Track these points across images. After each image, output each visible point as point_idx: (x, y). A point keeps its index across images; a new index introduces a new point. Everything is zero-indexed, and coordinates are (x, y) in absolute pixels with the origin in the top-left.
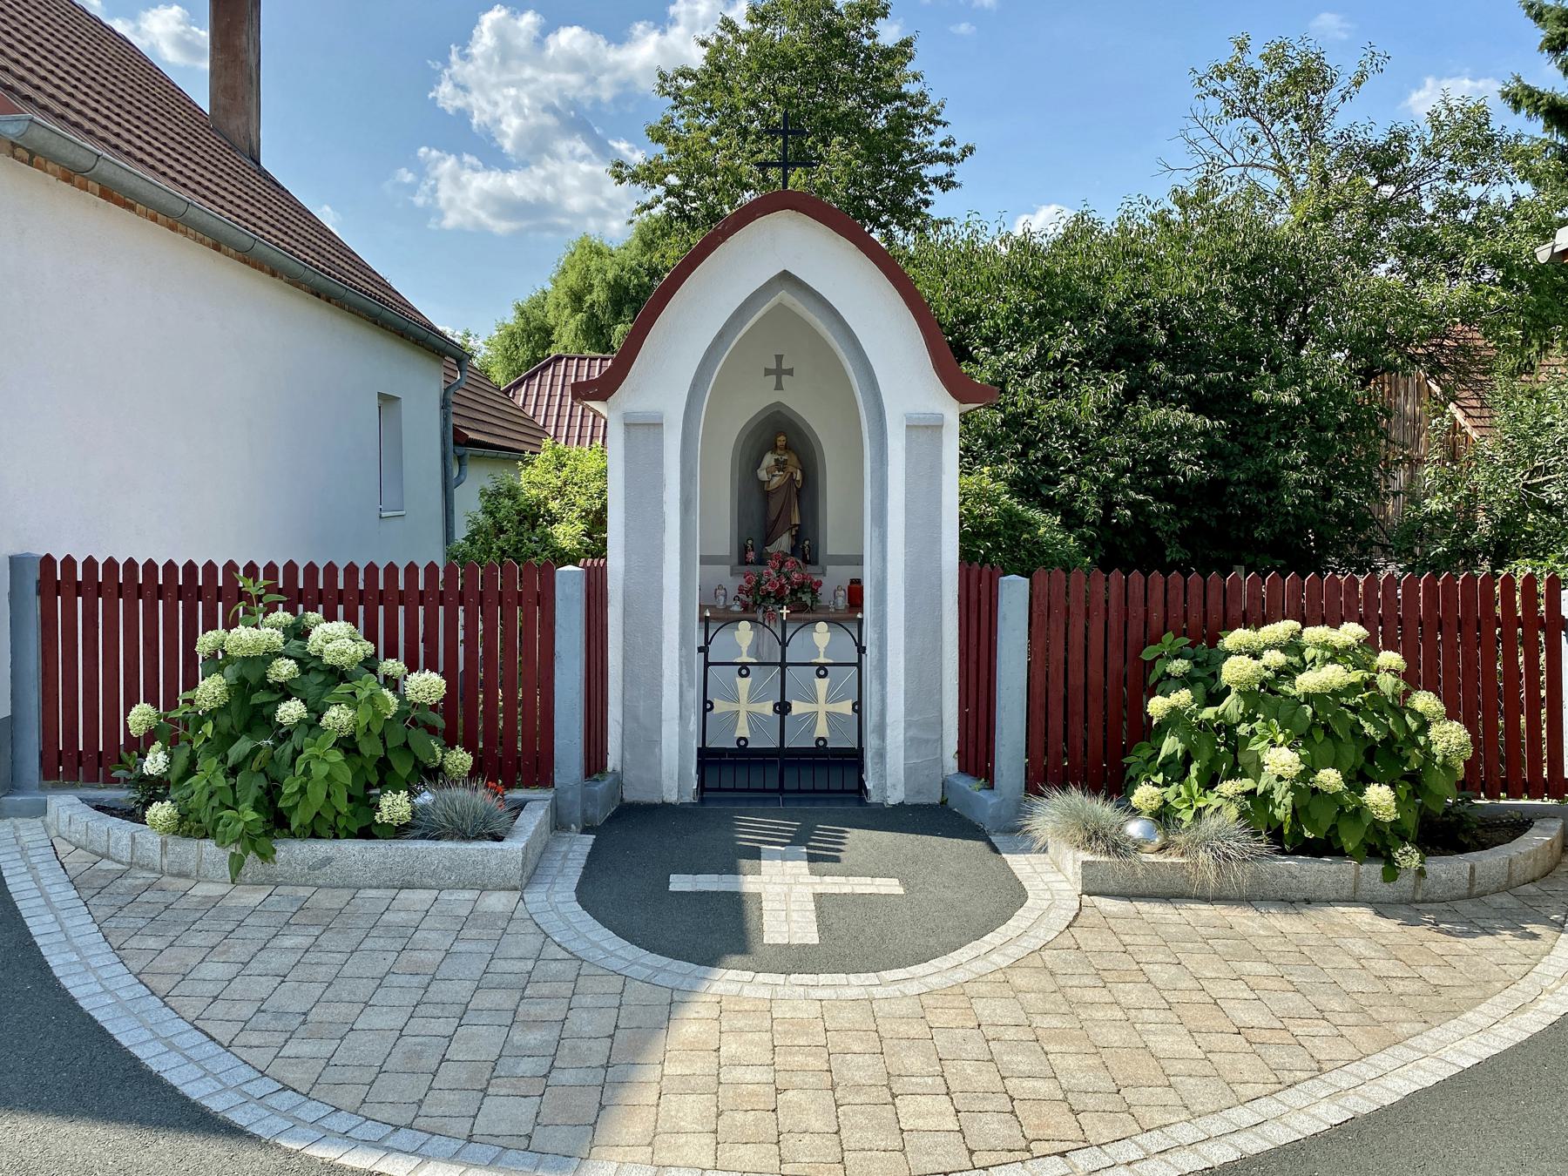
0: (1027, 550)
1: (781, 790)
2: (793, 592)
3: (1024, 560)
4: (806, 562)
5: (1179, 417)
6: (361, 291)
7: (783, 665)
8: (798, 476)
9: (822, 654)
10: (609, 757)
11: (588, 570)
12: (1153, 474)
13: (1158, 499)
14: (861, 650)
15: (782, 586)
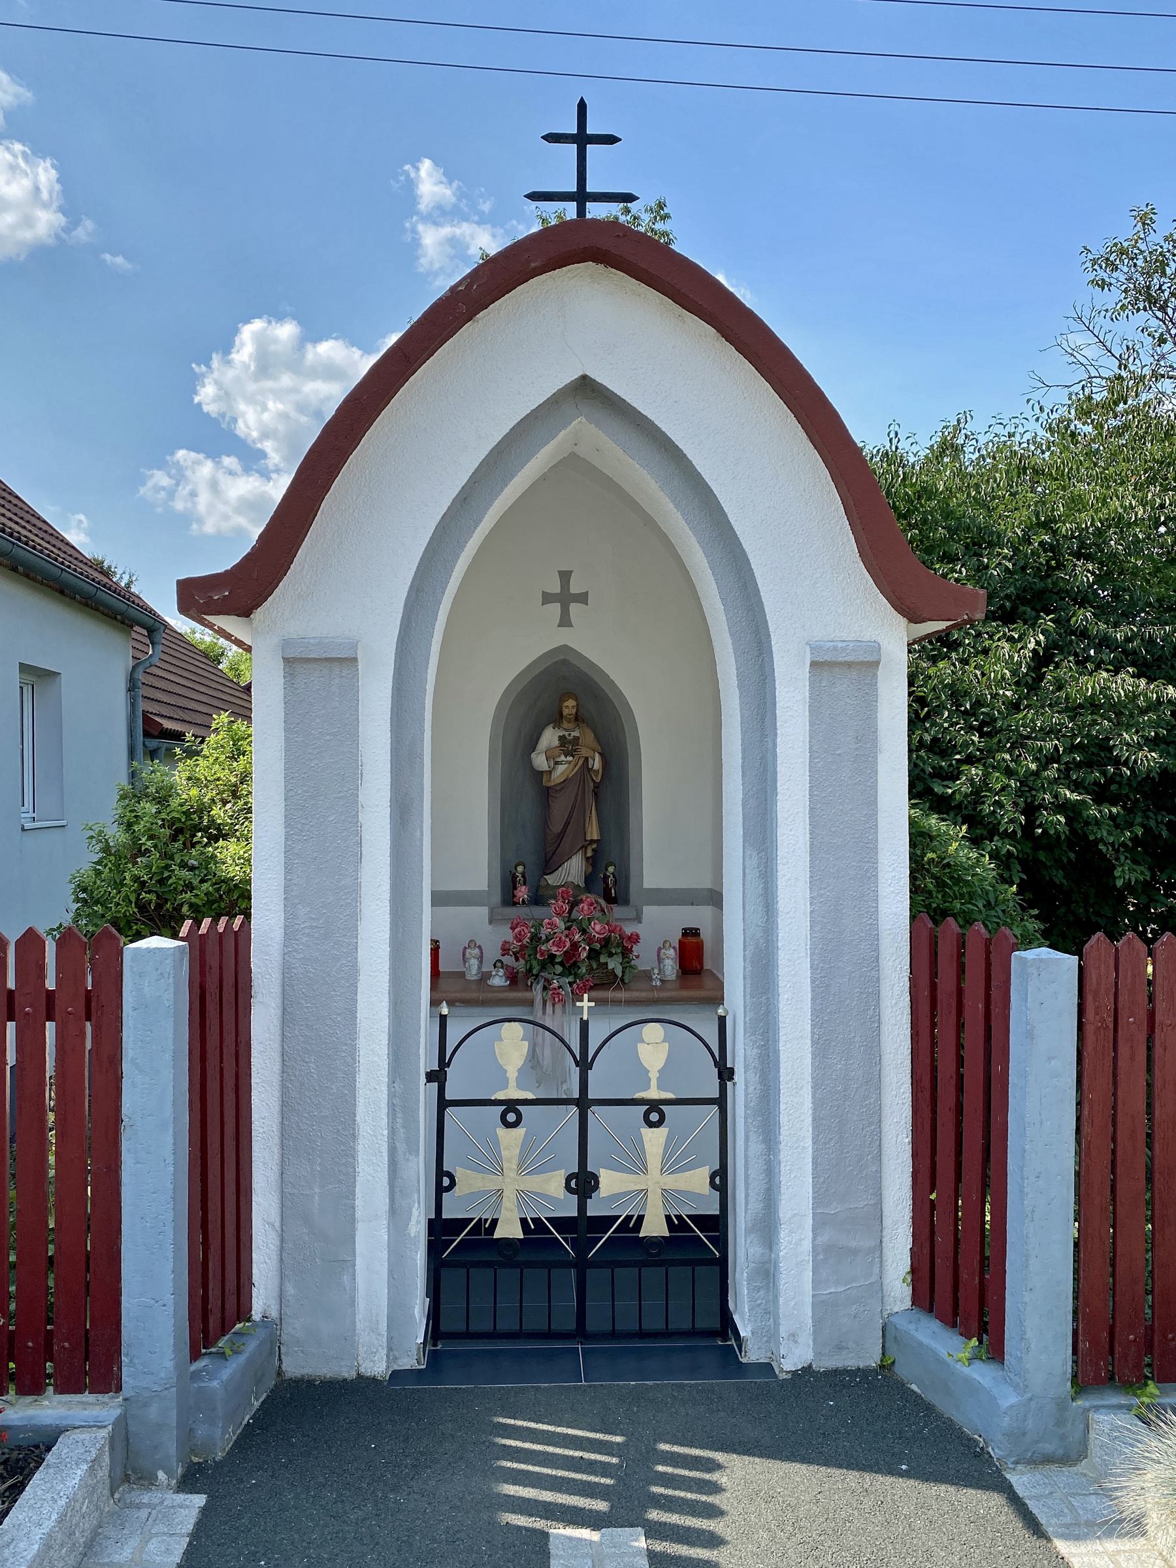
0: (933, 877)
1: (581, 1332)
2: (594, 954)
3: (930, 893)
4: (611, 900)
5: (1124, 684)
6: (138, 605)
7: (583, 1103)
8: (597, 764)
9: (654, 1083)
10: (255, 1291)
11: (200, 949)
12: (1088, 764)
13: (1098, 801)
14: (726, 1074)
15: (575, 946)
